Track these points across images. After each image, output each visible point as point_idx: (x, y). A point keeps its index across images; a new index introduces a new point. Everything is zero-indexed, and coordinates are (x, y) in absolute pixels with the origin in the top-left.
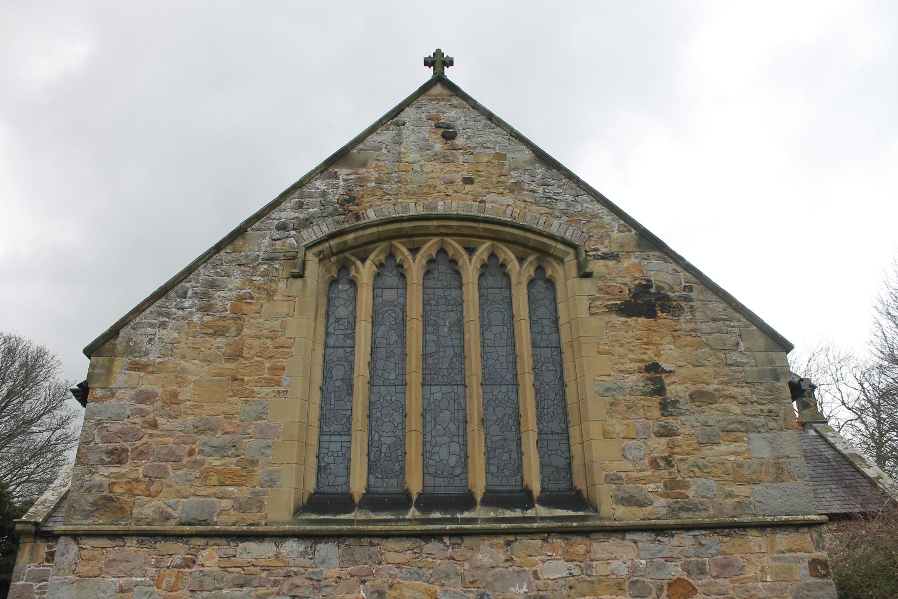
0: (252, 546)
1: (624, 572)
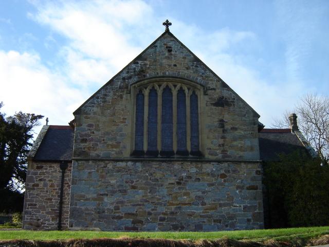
0: (121, 163)
1: (210, 172)
